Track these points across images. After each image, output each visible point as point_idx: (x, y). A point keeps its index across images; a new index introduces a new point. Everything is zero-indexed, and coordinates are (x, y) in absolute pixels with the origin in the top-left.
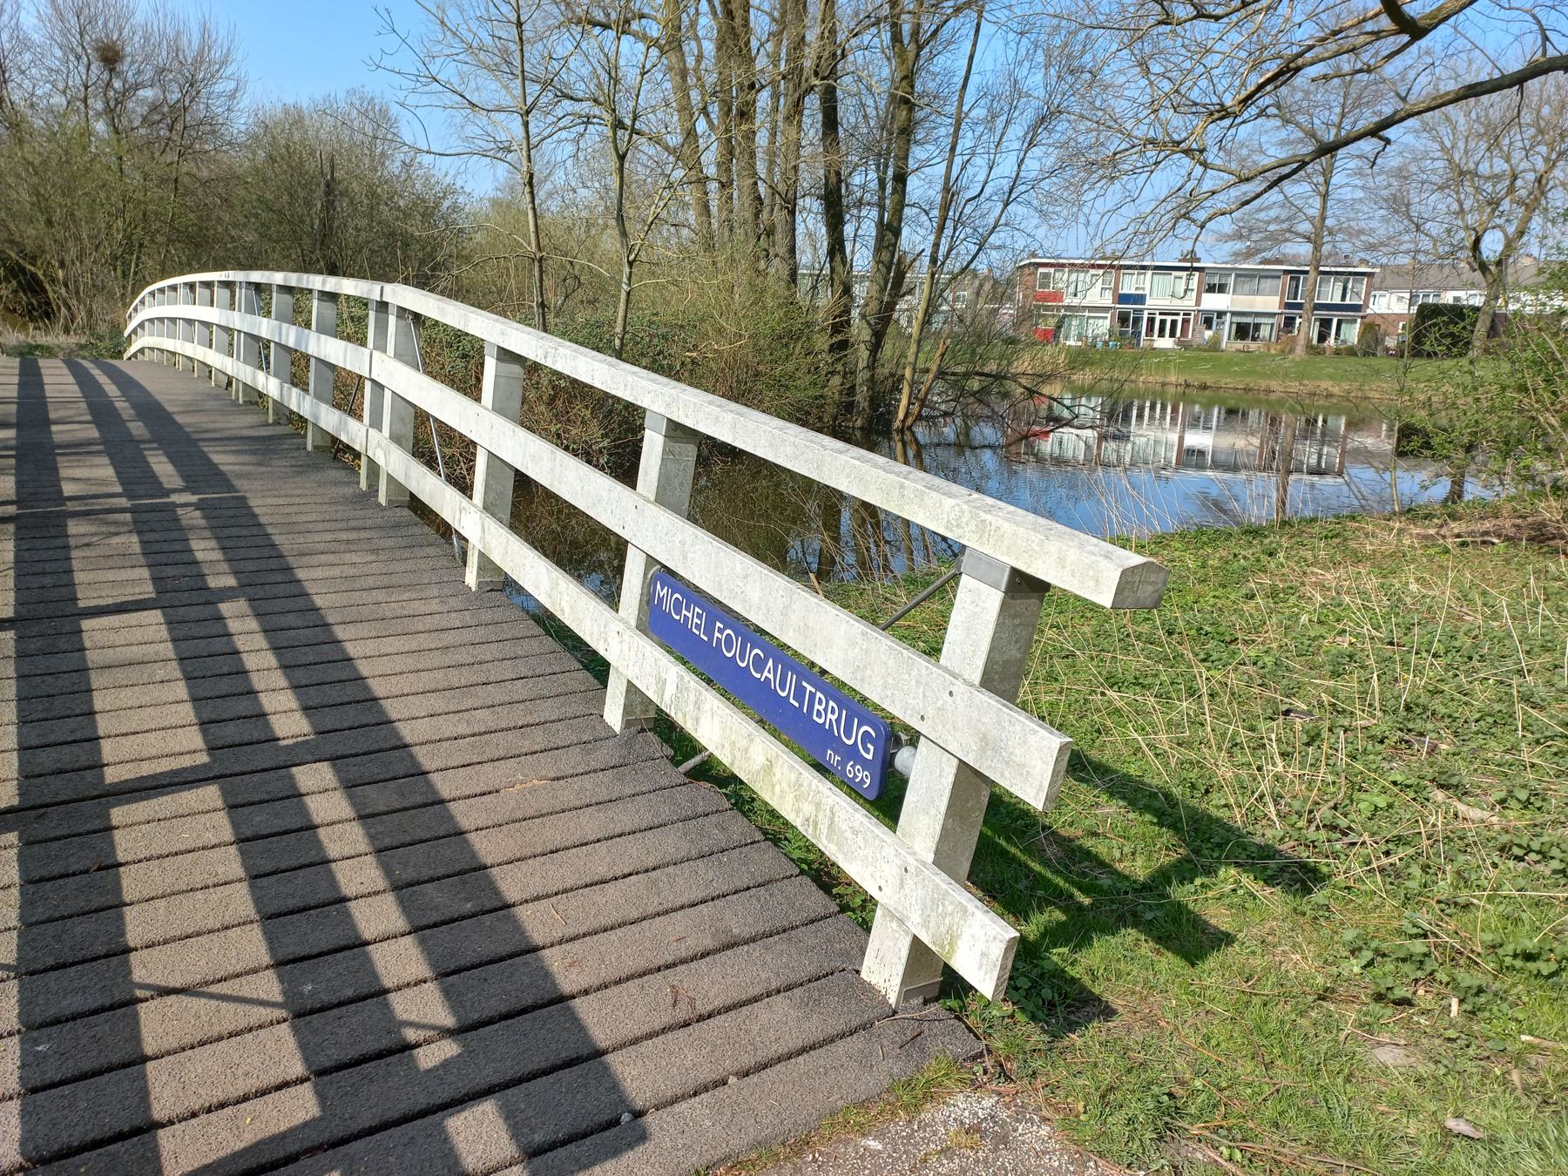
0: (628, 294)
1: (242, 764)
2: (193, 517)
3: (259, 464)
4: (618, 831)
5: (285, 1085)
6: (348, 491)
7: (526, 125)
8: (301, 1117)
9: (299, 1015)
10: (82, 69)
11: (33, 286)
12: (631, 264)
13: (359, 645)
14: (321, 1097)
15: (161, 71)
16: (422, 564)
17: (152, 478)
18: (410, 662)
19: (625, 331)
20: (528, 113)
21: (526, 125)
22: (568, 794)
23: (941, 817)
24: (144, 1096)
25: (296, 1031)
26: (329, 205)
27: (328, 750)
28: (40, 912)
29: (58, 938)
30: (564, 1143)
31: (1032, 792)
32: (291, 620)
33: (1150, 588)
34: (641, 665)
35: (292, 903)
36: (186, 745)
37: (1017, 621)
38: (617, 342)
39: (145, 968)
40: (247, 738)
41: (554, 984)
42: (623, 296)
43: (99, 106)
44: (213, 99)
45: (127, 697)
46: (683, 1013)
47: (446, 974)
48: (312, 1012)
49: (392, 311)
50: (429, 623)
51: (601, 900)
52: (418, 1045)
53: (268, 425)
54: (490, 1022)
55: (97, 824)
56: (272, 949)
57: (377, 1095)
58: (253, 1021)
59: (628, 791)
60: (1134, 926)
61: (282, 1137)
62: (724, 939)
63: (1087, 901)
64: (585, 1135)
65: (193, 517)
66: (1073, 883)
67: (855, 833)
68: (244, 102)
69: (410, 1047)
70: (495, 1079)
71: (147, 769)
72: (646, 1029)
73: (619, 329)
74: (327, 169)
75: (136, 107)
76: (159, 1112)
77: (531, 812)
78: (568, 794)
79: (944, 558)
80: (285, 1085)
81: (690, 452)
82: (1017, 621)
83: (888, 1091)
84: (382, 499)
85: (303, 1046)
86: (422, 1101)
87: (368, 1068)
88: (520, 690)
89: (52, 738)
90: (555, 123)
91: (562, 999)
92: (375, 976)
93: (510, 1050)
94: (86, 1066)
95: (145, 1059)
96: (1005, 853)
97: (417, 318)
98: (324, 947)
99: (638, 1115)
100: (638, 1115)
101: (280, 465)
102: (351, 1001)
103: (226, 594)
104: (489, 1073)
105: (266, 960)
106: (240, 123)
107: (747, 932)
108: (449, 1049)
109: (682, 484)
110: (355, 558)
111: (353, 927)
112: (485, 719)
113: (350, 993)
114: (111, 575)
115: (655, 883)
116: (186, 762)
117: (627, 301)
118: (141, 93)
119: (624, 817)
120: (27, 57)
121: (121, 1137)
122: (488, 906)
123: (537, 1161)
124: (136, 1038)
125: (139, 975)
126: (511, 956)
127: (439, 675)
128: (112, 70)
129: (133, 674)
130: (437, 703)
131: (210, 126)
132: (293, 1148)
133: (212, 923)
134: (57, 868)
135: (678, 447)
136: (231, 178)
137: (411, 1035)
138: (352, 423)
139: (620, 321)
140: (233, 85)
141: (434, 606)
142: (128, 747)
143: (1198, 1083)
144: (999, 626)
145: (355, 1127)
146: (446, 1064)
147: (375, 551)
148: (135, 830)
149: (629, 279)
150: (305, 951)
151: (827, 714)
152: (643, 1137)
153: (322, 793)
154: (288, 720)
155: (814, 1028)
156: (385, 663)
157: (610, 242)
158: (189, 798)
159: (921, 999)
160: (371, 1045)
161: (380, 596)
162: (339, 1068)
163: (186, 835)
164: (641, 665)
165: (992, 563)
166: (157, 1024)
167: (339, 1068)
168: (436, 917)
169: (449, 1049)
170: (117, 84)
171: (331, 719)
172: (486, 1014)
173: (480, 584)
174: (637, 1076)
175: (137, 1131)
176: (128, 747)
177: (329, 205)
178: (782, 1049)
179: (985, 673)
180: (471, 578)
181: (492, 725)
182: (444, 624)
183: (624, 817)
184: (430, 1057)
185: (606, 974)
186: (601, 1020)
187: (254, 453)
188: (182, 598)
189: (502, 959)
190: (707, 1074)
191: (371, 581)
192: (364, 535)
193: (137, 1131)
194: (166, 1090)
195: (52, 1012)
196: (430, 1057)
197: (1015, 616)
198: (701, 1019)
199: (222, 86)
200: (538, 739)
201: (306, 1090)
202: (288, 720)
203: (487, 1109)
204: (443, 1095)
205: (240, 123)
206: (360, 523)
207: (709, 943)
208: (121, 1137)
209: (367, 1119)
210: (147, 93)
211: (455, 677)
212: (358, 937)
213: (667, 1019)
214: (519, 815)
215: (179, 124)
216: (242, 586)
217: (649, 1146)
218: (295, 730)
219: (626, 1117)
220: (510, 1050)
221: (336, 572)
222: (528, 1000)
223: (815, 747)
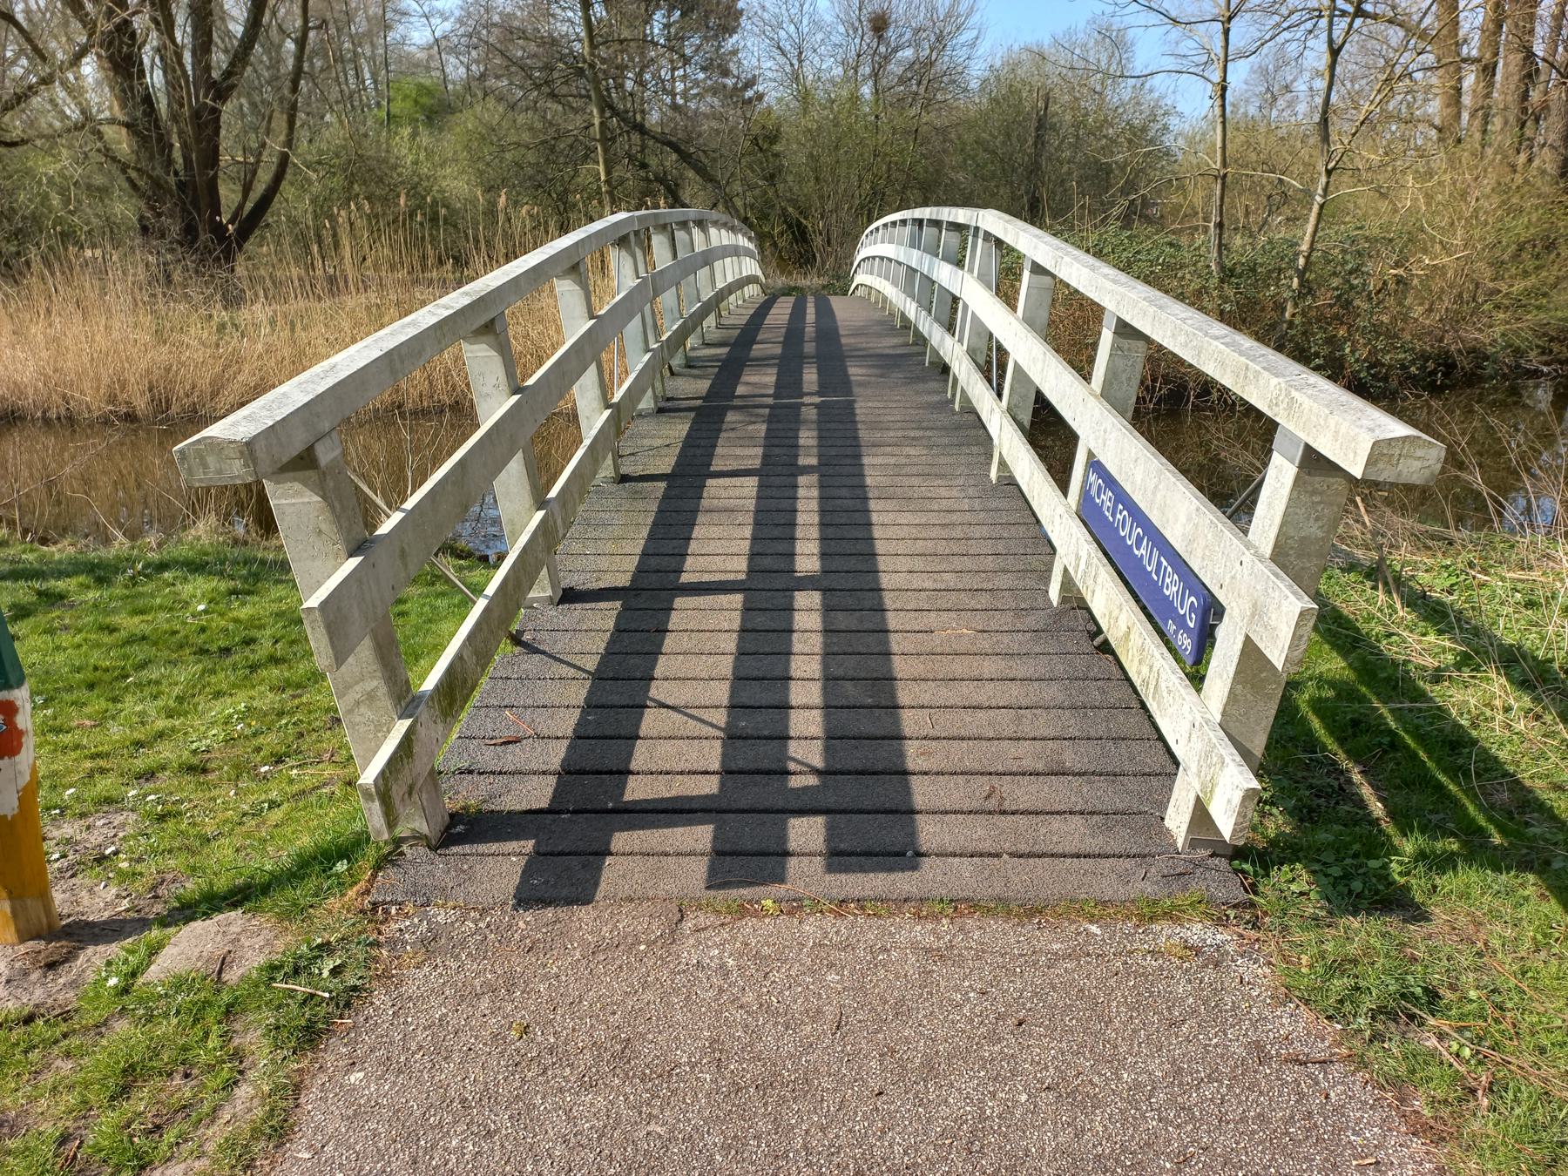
0: (1322, 206)
1: (766, 588)
2: (810, 414)
3: (882, 376)
4: (1011, 676)
5: (707, 773)
6: (936, 398)
7: (1226, 32)
8: (707, 791)
9: (730, 738)
10: (857, 41)
11: (800, 234)
12: (1329, 173)
13: (882, 516)
14: (722, 784)
15: (917, 31)
16: (963, 459)
17: (798, 382)
18: (914, 532)
19: (1312, 249)
20: (1230, 19)
21: (1226, 32)
22: (985, 644)
23: (1230, 681)
24: (630, 755)
25: (724, 745)
26: (1039, 141)
27: (825, 584)
28: (616, 648)
29: (620, 664)
30: (859, 855)
31: (1277, 653)
32: (844, 492)
33: (1418, 464)
34: (1073, 546)
35: (756, 673)
36: (738, 567)
37: (1317, 499)
38: (1301, 261)
39: (657, 691)
40: (775, 567)
41: (903, 763)
42: (1316, 208)
43: (868, 70)
44: (957, 51)
45: (715, 531)
46: (992, 804)
47: (832, 737)
48: (739, 738)
49: (981, 234)
50: (945, 504)
51: (968, 719)
52: (794, 773)
53: (907, 345)
54: (849, 773)
55: (665, 605)
56: (732, 696)
57: (756, 793)
58: (703, 734)
59: (1037, 649)
60: (1539, 873)
61: (693, 798)
62: (1056, 768)
63: (1497, 839)
64: (876, 855)
65: (810, 414)
66: (1491, 819)
67: (1169, 692)
68: (983, 48)
69: (789, 773)
70: (833, 806)
71: (706, 578)
72: (957, 807)
73: (1305, 247)
74: (1041, 104)
75: (894, 68)
76: (633, 766)
77: (948, 650)
78: (985, 644)
79: (1260, 431)
80: (707, 773)
81: (1139, 351)
82: (1318, 499)
83: (1133, 901)
84: (957, 407)
85: (724, 755)
86: (780, 804)
87: (758, 777)
88: (990, 562)
89: (662, 551)
90: (1278, 25)
91: (906, 773)
92: (787, 727)
93: (849, 791)
94: (608, 733)
95: (638, 737)
96: (1440, 787)
97: (999, 243)
98: (764, 703)
99: (919, 854)
100: (919, 854)
101: (897, 375)
102: (766, 738)
103: (807, 470)
104: (831, 801)
105: (725, 702)
106: (976, 71)
107: (1078, 767)
108: (812, 780)
109: (1129, 379)
110: (912, 452)
111: (787, 696)
112: (950, 580)
113: (766, 733)
114: (738, 451)
115: (1019, 718)
116: (731, 577)
117: (1320, 215)
118: (900, 53)
119: (1022, 669)
120: (819, 36)
121: (611, 773)
122: (884, 703)
123: (836, 859)
124: (638, 726)
125: (653, 693)
126: (883, 738)
127: (930, 544)
128: (880, 37)
129: (724, 517)
130: (918, 564)
131: (954, 76)
132: (695, 806)
133: (704, 675)
134: (633, 626)
135: (1126, 343)
136: (970, 124)
137: (792, 766)
138: (948, 337)
139: (1308, 238)
140: (975, 33)
141: (954, 493)
142: (702, 562)
143: (1473, 994)
144: (1291, 500)
145: (734, 806)
146: (806, 789)
147: (930, 447)
148: (684, 613)
149: (1325, 190)
150: (752, 703)
151: (1172, 587)
152: (915, 868)
153: (808, 612)
154: (807, 559)
155: (1093, 844)
156: (894, 532)
157: (1309, 150)
158: (724, 600)
159: (1209, 852)
160: (765, 764)
161: (916, 481)
162: (741, 772)
163: (713, 621)
164: (1073, 546)
165: (1293, 438)
166: (651, 721)
167: (741, 772)
168: (844, 702)
169: (812, 780)
170: (882, 49)
171: (837, 564)
172: (848, 767)
173: (999, 478)
174: (929, 832)
175: (620, 772)
176: (702, 562)
177: (1039, 141)
178: (1059, 849)
179: (1276, 546)
180: (993, 475)
181: (952, 585)
182: (956, 507)
183: (1022, 669)
184: (795, 782)
185: (943, 766)
186: (922, 792)
187: (881, 367)
188: (777, 475)
189: (876, 738)
190: (986, 846)
191: (914, 470)
192: (928, 433)
193: (620, 772)
194: (641, 756)
195: (603, 701)
196: (795, 782)
197: (1313, 493)
198: (1004, 813)
199: (966, 36)
200: (984, 600)
201: (715, 779)
202: (807, 559)
203: (819, 821)
204: (794, 805)
205: (976, 71)
206: (931, 424)
207: (1040, 767)
208: (611, 773)
209: (743, 804)
210: (908, 53)
211: (942, 547)
212: (787, 702)
213: (975, 805)
214: (939, 650)
215: (927, 77)
216: (820, 464)
217: (916, 874)
218: (809, 567)
219: (909, 854)
220: (849, 791)
221: (892, 460)
222: (880, 767)
223: (1153, 610)
